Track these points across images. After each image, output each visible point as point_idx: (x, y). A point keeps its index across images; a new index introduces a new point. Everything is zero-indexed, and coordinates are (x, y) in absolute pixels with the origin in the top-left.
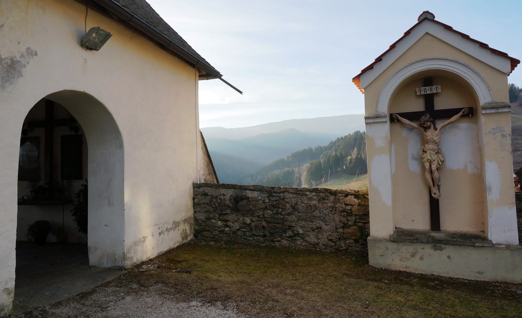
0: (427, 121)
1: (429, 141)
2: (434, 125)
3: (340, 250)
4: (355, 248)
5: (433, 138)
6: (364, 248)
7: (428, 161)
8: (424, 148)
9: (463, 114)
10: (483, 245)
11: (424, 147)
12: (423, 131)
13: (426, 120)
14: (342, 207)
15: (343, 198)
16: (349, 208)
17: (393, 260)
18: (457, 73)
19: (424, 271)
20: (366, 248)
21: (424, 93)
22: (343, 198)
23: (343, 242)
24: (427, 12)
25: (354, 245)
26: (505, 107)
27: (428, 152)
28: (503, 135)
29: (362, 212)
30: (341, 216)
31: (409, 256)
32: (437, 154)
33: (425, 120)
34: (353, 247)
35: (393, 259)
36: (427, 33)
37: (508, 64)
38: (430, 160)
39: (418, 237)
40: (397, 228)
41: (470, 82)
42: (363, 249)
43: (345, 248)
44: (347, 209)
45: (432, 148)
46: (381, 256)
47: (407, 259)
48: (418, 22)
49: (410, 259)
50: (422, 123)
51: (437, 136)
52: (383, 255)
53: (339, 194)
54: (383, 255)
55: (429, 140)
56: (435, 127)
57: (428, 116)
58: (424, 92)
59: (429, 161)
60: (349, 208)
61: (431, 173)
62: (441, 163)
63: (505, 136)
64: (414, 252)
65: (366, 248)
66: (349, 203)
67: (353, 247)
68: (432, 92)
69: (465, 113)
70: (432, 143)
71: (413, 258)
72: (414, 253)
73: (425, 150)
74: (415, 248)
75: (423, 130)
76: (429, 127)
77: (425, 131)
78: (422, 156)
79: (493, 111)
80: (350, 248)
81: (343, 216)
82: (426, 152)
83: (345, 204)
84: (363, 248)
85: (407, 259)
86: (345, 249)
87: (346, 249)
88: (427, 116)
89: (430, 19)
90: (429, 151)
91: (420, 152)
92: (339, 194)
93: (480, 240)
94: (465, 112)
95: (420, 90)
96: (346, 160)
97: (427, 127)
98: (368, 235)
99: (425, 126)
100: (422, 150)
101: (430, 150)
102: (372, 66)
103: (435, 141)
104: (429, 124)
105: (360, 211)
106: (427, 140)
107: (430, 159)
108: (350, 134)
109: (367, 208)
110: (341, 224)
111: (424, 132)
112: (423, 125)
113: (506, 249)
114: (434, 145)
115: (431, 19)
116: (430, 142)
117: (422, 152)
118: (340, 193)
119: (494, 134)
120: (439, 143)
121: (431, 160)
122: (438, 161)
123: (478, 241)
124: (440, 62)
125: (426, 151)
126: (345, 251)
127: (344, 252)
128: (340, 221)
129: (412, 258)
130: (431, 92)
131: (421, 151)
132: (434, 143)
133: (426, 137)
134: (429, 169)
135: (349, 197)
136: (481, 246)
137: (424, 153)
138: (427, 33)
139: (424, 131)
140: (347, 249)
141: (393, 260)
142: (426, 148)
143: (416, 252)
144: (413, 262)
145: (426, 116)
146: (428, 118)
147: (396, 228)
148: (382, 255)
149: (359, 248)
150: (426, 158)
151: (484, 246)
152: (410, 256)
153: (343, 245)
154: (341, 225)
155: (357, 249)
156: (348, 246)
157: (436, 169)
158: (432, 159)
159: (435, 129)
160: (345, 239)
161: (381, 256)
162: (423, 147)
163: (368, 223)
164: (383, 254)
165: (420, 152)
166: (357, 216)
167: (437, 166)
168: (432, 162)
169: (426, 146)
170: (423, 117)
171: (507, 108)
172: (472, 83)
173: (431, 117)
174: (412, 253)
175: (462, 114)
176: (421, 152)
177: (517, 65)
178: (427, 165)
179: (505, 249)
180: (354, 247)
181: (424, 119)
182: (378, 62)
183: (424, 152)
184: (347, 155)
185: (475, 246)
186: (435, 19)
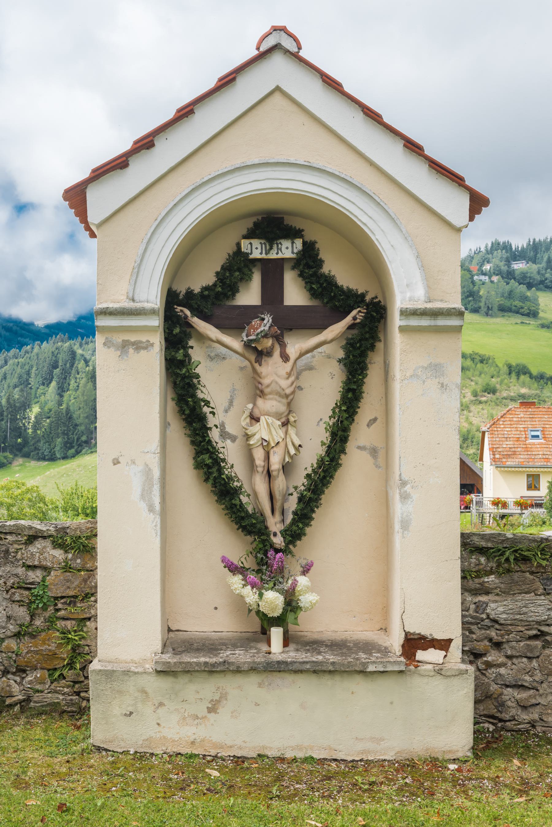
0: (266, 336)
1: (267, 391)
2: (283, 346)
3: (7, 703)
4: (50, 695)
5: (277, 383)
6: (78, 694)
7: (262, 444)
8: (253, 409)
9: (353, 321)
10: (386, 667)
11: (255, 404)
12: (253, 361)
13: (261, 332)
14: (17, 575)
15: (21, 549)
16: (35, 576)
17: (158, 724)
18: (347, 210)
19: (240, 748)
20: (82, 694)
21: (259, 256)
22: (21, 547)
23: (15, 681)
24: (283, 29)
25: (47, 686)
26: (451, 315)
27: (262, 419)
28: (442, 385)
29: (75, 589)
30: (14, 601)
31: (202, 710)
32: (286, 427)
33: (259, 330)
34: (46, 691)
35: (159, 722)
36: (278, 89)
37: (465, 201)
38: (266, 441)
39: (227, 656)
40: (172, 631)
41: (377, 240)
42: (74, 698)
43: (21, 697)
44: (31, 581)
45: (274, 410)
46: (125, 715)
47: (197, 718)
48: (256, 52)
49: (204, 718)
50: (251, 340)
51: (288, 378)
52: (131, 713)
53: (7, 537)
54: (131, 713)
55: (268, 386)
56: (285, 351)
57: (268, 319)
58: (261, 253)
59: (265, 444)
60: (35, 576)
61: (267, 478)
62: (292, 451)
63: (446, 389)
64: (217, 697)
65: (82, 694)
66: (36, 563)
67: (46, 691)
68: (280, 256)
69: (358, 321)
70: (275, 396)
71: (212, 714)
72: (216, 700)
73: (256, 413)
74: (218, 688)
75: (253, 357)
76: (269, 353)
77: (259, 361)
78: (246, 429)
79: (425, 322)
80: (36, 697)
81: (18, 601)
82: (258, 420)
83: (24, 565)
84: (75, 692)
85: (197, 718)
86: (20, 702)
87: (24, 700)
88: (265, 322)
89: (288, 51)
90: (266, 417)
91: (243, 418)
92: (7, 537)
93: (379, 655)
94: (357, 316)
95: (249, 246)
96: (25, 418)
97: (265, 351)
98: (92, 653)
99: (260, 349)
100: (247, 413)
101: (269, 416)
102: (124, 159)
103: (283, 390)
104: (269, 342)
105: (68, 584)
106: (263, 387)
107: (267, 439)
108: (359, 408)
109: (89, 577)
110: (11, 627)
111: (257, 365)
112: (253, 345)
113: (436, 674)
114: (279, 402)
115: (291, 50)
116: (270, 393)
117: (248, 420)
118: (11, 533)
119: (424, 382)
120: (291, 397)
121: (269, 443)
122: (286, 446)
123: (373, 659)
124: (155, 247)
125: (259, 416)
126: (21, 707)
127: (17, 708)
128: (9, 618)
129: (209, 715)
130: (277, 253)
131: (245, 416)
132: (280, 396)
133: (260, 378)
134: (264, 467)
135: (39, 544)
136: (380, 672)
137: (253, 421)
138: (278, 89)
139: (256, 362)
140: (28, 700)
141: (158, 724)
142: (258, 408)
143: (221, 697)
144: (212, 725)
145: (263, 319)
146: (268, 325)
147: (170, 630)
148: (128, 713)
149: (63, 694)
150: (257, 437)
151: (387, 671)
152: (206, 710)
153: (16, 689)
154: (12, 628)
155: (58, 698)
156: (31, 692)
157: (281, 467)
158: (273, 440)
159: (285, 358)
160: (21, 671)
161: (125, 715)
162: (250, 406)
163: (92, 619)
164: (130, 709)
165: (243, 418)
166: (62, 601)
167: (284, 460)
168: (273, 447)
169: (260, 402)
170: (255, 322)
171: (454, 317)
172: (380, 243)
173: (275, 322)
174: (212, 700)
175: (350, 324)
176: (245, 418)
177: (482, 209)
178: (259, 455)
179: (432, 673)
180: (49, 693)
181: (257, 329)
182: (142, 151)
183: (254, 419)
184: (26, 406)
185: (366, 672)
186: (302, 54)
